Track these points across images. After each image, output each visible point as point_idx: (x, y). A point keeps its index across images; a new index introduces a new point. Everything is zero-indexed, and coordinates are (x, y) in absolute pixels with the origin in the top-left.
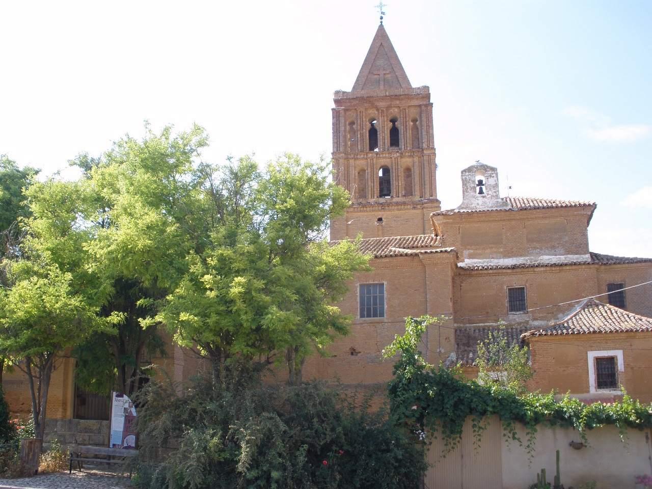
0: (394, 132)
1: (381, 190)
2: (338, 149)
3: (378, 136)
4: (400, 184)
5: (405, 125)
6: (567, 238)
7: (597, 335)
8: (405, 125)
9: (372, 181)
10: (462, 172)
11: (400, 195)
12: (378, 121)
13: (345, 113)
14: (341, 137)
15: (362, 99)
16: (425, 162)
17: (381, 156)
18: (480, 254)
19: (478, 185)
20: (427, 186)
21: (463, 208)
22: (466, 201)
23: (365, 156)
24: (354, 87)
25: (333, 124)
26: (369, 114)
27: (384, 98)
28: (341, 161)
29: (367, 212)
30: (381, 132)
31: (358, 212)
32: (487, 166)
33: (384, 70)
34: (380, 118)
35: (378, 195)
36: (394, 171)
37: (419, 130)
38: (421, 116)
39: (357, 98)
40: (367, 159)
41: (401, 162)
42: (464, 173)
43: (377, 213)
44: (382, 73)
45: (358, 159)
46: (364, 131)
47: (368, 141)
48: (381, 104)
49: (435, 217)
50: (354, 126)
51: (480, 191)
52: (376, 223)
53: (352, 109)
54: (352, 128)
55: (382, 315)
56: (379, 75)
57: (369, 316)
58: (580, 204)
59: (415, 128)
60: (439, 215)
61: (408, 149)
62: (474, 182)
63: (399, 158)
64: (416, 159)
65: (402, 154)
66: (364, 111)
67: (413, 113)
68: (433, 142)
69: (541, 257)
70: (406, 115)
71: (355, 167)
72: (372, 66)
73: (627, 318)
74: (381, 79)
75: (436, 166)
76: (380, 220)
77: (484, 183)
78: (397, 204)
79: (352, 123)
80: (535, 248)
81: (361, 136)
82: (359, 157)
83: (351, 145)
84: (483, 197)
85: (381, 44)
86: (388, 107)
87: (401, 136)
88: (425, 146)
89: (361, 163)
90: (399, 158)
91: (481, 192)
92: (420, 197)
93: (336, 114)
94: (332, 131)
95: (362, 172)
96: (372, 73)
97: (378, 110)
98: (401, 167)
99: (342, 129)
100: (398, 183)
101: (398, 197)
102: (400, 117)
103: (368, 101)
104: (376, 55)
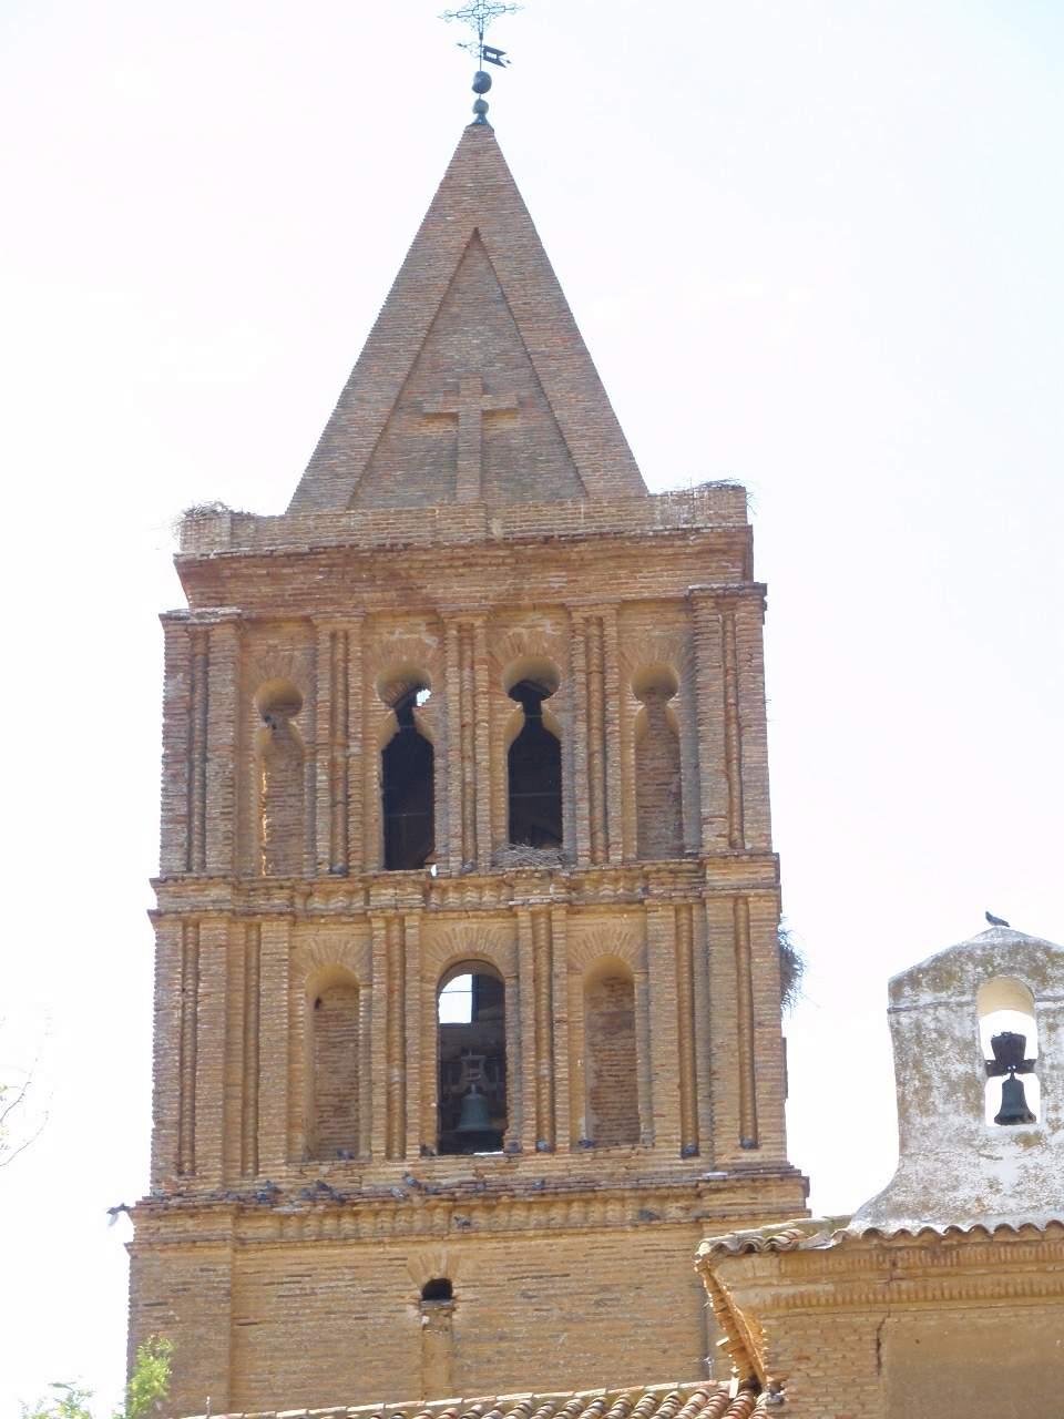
0: (535, 764)
1: (450, 1110)
2: (196, 856)
3: (438, 778)
4: (562, 1073)
5: (596, 713)
8: (596, 713)
9: (396, 1051)
10: (896, 988)
11: (563, 1140)
12: (439, 694)
13: (244, 646)
14: (214, 786)
15: (346, 560)
16: (713, 938)
17: (453, 898)
19: (994, 1069)
20: (727, 1087)
21: (898, 1211)
22: (920, 1167)
23: (358, 903)
24: (302, 491)
25: (169, 708)
26: (388, 650)
27: (466, 559)
28: (214, 930)
29: (360, 1241)
30: (454, 757)
31: (301, 1242)
32: (1047, 950)
33: (486, 390)
34: (452, 673)
35: (431, 1140)
36: (527, 988)
37: (683, 746)
38: (693, 662)
39: (312, 551)
40: (364, 918)
41: (568, 936)
42: (907, 991)
43: (420, 1249)
44: (471, 405)
45: (311, 917)
46: (355, 749)
47: (376, 811)
48: (457, 588)
49: (731, 1266)
50: (298, 723)
51: (1005, 1105)
52: (412, 1312)
53: (289, 620)
54: (280, 734)
56: (454, 417)
58: (653, 1094)
59: (661, 736)
60: (750, 1250)
61: (616, 857)
62: (969, 1046)
63: (558, 914)
64: (661, 921)
65: (574, 886)
66: (354, 629)
67: (647, 643)
68: (765, 819)
70: (603, 658)
71: (294, 970)
72: (415, 365)
74: (462, 447)
75: (787, 966)
76: (438, 1291)
77: (1030, 1053)
78: (544, 1193)
79: (284, 706)
81: (333, 782)
82: (317, 903)
83: (280, 834)
84: (1028, 1141)
85: (476, 233)
86: (502, 612)
87: (574, 783)
88: (713, 839)
89: (332, 943)
90: (558, 914)
91: (1015, 1110)
92: (685, 1154)
93: (189, 647)
94: (161, 750)
95: (334, 1002)
96: (417, 409)
97: (437, 625)
98: (571, 969)
99: (223, 735)
100: (552, 1070)
101: (552, 1149)
102: (572, 671)
103: (382, 569)
104: (443, 303)
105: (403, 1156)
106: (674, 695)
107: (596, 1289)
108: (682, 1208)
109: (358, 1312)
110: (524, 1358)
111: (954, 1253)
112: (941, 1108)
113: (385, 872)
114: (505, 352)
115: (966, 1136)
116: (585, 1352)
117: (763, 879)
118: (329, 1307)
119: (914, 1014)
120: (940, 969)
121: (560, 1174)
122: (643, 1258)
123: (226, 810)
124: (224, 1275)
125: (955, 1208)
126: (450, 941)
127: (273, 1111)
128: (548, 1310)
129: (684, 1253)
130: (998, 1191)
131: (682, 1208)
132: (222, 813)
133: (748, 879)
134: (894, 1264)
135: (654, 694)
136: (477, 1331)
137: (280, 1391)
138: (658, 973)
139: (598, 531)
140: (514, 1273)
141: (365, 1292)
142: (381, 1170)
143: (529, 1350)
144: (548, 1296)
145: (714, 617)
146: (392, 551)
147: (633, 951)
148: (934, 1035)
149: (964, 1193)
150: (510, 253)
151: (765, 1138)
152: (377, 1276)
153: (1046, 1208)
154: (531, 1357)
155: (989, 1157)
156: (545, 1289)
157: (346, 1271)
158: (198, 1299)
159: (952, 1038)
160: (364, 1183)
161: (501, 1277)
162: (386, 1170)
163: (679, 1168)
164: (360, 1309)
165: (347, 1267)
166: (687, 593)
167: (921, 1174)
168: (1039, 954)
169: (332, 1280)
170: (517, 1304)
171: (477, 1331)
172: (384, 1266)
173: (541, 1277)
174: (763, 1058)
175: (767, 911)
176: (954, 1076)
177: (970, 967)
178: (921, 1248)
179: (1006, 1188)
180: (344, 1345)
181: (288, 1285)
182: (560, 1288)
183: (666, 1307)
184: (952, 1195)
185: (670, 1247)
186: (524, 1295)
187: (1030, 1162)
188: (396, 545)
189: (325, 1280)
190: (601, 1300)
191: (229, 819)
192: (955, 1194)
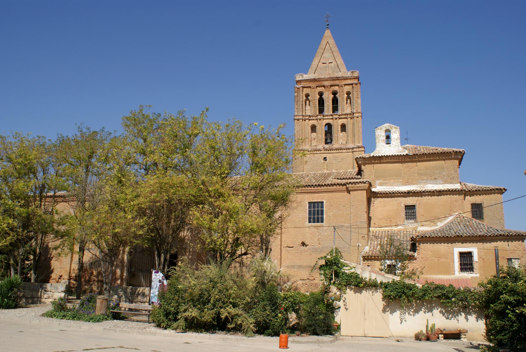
6: (445, 173)
7: (460, 238)
18: (387, 183)
55: (322, 221)
57: (314, 222)
69: (427, 185)
73: (482, 227)
76: (325, 159)
80: (423, 179)
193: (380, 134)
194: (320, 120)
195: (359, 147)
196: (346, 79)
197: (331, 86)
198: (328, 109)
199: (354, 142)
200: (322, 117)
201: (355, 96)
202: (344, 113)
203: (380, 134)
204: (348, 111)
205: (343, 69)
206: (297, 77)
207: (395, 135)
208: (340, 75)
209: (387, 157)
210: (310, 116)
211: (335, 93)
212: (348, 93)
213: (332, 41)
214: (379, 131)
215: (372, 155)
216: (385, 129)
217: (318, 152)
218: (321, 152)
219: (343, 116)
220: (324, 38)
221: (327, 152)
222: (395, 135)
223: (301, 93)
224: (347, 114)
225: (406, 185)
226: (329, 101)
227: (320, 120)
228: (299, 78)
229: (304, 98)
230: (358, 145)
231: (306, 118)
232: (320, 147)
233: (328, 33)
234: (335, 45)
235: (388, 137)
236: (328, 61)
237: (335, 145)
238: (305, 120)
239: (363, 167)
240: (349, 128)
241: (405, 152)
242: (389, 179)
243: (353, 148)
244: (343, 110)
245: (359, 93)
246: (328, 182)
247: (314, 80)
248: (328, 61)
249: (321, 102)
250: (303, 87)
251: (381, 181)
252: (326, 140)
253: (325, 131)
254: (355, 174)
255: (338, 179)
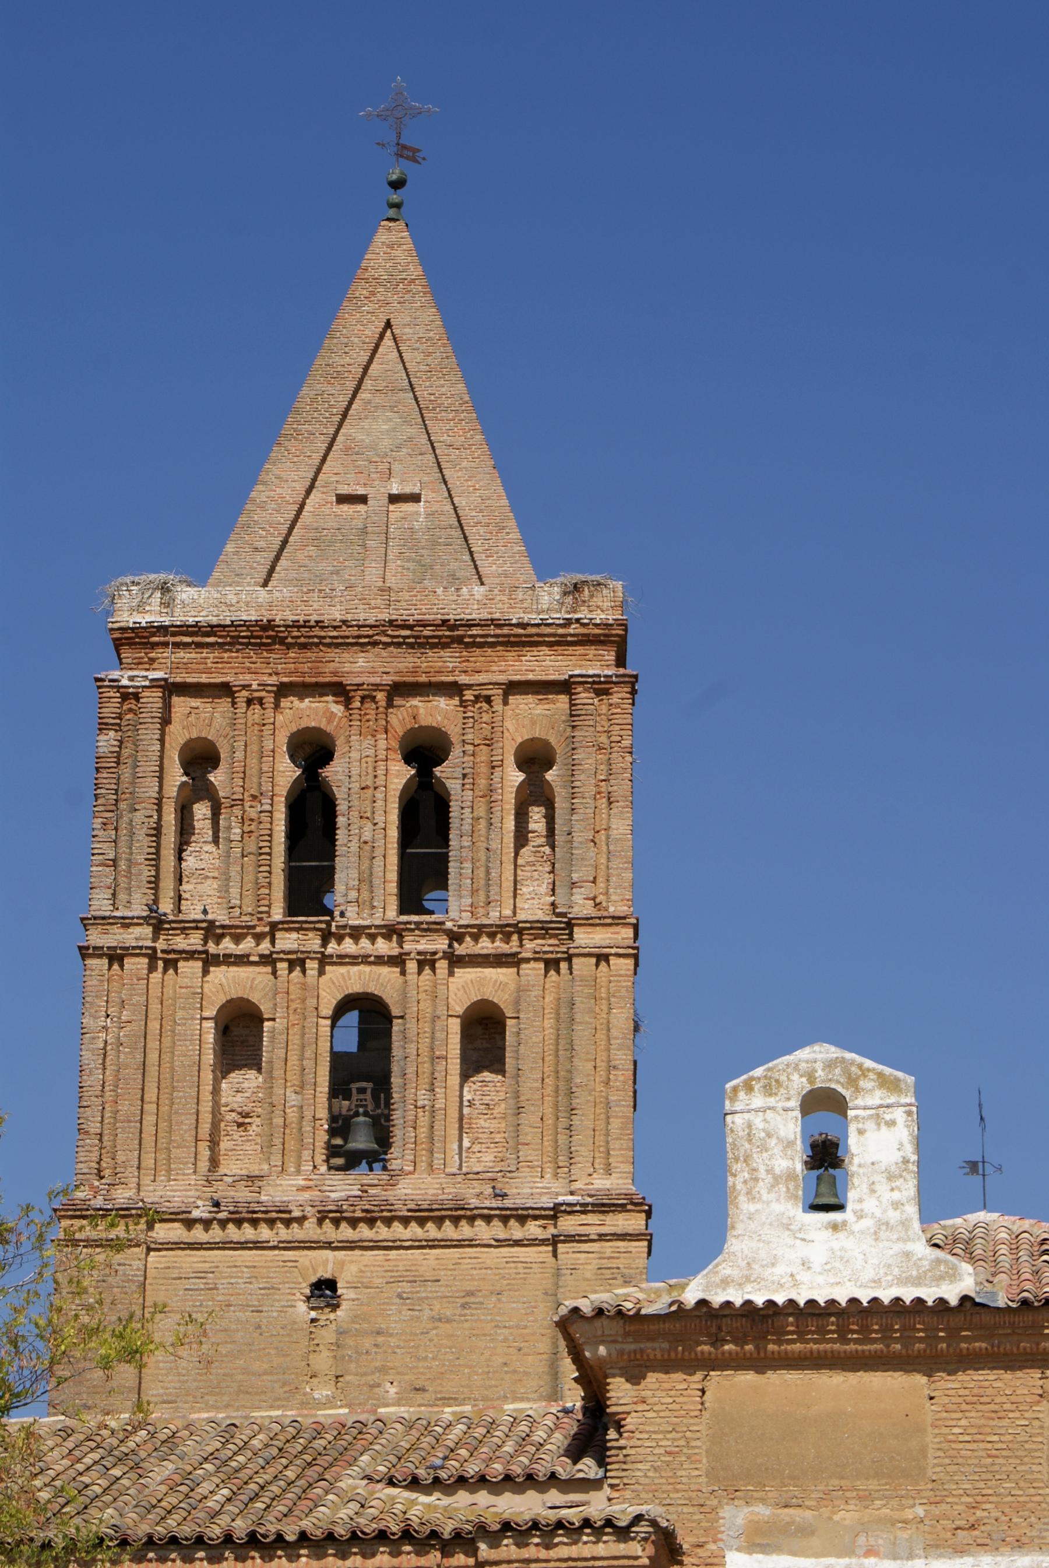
18: (805, 1531)
52: (302, 1307)
76: (325, 1290)
105: (298, 1172)
106: (551, 768)
107: (463, 1294)
108: (540, 1226)
109: (253, 1306)
110: (398, 1351)
111: (770, 1321)
112: (765, 1196)
113: (289, 919)
114: (410, 439)
115: (785, 1221)
116: (450, 1348)
117: (623, 939)
118: (229, 1300)
119: (746, 1116)
120: (771, 1078)
121: (435, 1191)
122: (505, 1268)
123: (150, 857)
124: (138, 1270)
125: (773, 1282)
126: (345, 981)
127: (184, 1127)
128: (420, 1310)
129: (540, 1265)
130: (809, 1268)
131: (540, 1226)
132: (146, 859)
133: (610, 939)
134: (720, 1328)
135: (534, 763)
136: (357, 1326)
137: (184, 1372)
138: (527, 1019)
139: (489, 617)
140: (392, 1277)
141: (261, 1289)
142: (278, 1182)
143: (402, 1344)
144: (420, 1299)
145: (591, 701)
146: (304, 627)
147: (507, 996)
148: (763, 1135)
149: (780, 1270)
150: (418, 345)
151: (616, 1168)
152: (272, 1275)
153: (848, 1284)
154: (403, 1351)
155: (804, 1240)
156: (418, 1292)
157: (245, 1270)
158: (115, 1290)
159: (778, 1138)
160: (263, 1193)
161: (381, 1280)
162: (282, 1182)
163: (538, 1190)
164: (256, 1303)
165: (246, 1267)
166: (567, 677)
167: (746, 1251)
168: (853, 1069)
169: (232, 1277)
170: (393, 1304)
171: (357, 1326)
172: (278, 1267)
173: (415, 1282)
174: (615, 1098)
175: (625, 967)
176: (777, 1171)
177: (795, 1077)
178: (742, 1316)
179: (816, 1267)
180: (240, 1334)
181: (194, 1280)
182: (431, 1292)
183: (523, 1311)
184: (770, 1270)
185: (528, 1260)
186: (400, 1296)
187: (836, 1245)
188: (309, 621)
189: (226, 1278)
190: (467, 1303)
191: (152, 866)
192: (774, 1270)
193: (766, 1122)
194: (297, 963)
195: (604, 1207)
196: (520, 638)
197: (401, 690)
198: (366, 880)
199: (563, 1161)
200: (314, 942)
201: (586, 784)
202: (493, 917)
203: (766, 1122)
204: (533, 908)
205: (505, 555)
206: (125, 601)
207: (881, 1143)
208: (471, 602)
209: (813, 1315)
210: (212, 931)
211: (424, 752)
212: (535, 759)
213: (420, 321)
214: (758, 1101)
215: (691, 1296)
216: (799, 1085)
217: (264, 1233)
218: (296, 1232)
219: (485, 946)
220: (360, 290)
221: (346, 1232)
222: (881, 1143)
223: (149, 734)
224: (507, 930)
225: (960, 1551)
226: (367, 806)
227: (297, 963)
228: (135, 607)
229: (176, 776)
230: (601, 1183)
231: (181, 943)
232: (286, 1189)
233: (391, 249)
234: (442, 353)
235: (825, 1156)
236: (384, 489)
237: (414, 1184)
238: (171, 964)
239: (620, 1392)
240: (528, 1039)
241: (953, 1276)
242: (827, 1498)
243: (556, 1212)
244: (484, 889)
245: (622, 762)
246: (334, 1513)
247: (264, 636)
248: (384, 489)
249: (312, 817)
250: (171, 689)
251: (763, 1511)
252: (340, 1126)
253: (337, 1058)
254: (559, 1440)
255: (414, 1483)
